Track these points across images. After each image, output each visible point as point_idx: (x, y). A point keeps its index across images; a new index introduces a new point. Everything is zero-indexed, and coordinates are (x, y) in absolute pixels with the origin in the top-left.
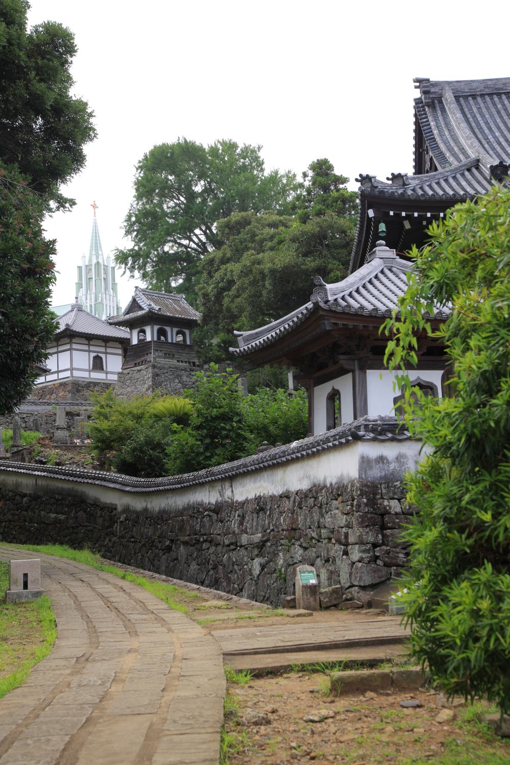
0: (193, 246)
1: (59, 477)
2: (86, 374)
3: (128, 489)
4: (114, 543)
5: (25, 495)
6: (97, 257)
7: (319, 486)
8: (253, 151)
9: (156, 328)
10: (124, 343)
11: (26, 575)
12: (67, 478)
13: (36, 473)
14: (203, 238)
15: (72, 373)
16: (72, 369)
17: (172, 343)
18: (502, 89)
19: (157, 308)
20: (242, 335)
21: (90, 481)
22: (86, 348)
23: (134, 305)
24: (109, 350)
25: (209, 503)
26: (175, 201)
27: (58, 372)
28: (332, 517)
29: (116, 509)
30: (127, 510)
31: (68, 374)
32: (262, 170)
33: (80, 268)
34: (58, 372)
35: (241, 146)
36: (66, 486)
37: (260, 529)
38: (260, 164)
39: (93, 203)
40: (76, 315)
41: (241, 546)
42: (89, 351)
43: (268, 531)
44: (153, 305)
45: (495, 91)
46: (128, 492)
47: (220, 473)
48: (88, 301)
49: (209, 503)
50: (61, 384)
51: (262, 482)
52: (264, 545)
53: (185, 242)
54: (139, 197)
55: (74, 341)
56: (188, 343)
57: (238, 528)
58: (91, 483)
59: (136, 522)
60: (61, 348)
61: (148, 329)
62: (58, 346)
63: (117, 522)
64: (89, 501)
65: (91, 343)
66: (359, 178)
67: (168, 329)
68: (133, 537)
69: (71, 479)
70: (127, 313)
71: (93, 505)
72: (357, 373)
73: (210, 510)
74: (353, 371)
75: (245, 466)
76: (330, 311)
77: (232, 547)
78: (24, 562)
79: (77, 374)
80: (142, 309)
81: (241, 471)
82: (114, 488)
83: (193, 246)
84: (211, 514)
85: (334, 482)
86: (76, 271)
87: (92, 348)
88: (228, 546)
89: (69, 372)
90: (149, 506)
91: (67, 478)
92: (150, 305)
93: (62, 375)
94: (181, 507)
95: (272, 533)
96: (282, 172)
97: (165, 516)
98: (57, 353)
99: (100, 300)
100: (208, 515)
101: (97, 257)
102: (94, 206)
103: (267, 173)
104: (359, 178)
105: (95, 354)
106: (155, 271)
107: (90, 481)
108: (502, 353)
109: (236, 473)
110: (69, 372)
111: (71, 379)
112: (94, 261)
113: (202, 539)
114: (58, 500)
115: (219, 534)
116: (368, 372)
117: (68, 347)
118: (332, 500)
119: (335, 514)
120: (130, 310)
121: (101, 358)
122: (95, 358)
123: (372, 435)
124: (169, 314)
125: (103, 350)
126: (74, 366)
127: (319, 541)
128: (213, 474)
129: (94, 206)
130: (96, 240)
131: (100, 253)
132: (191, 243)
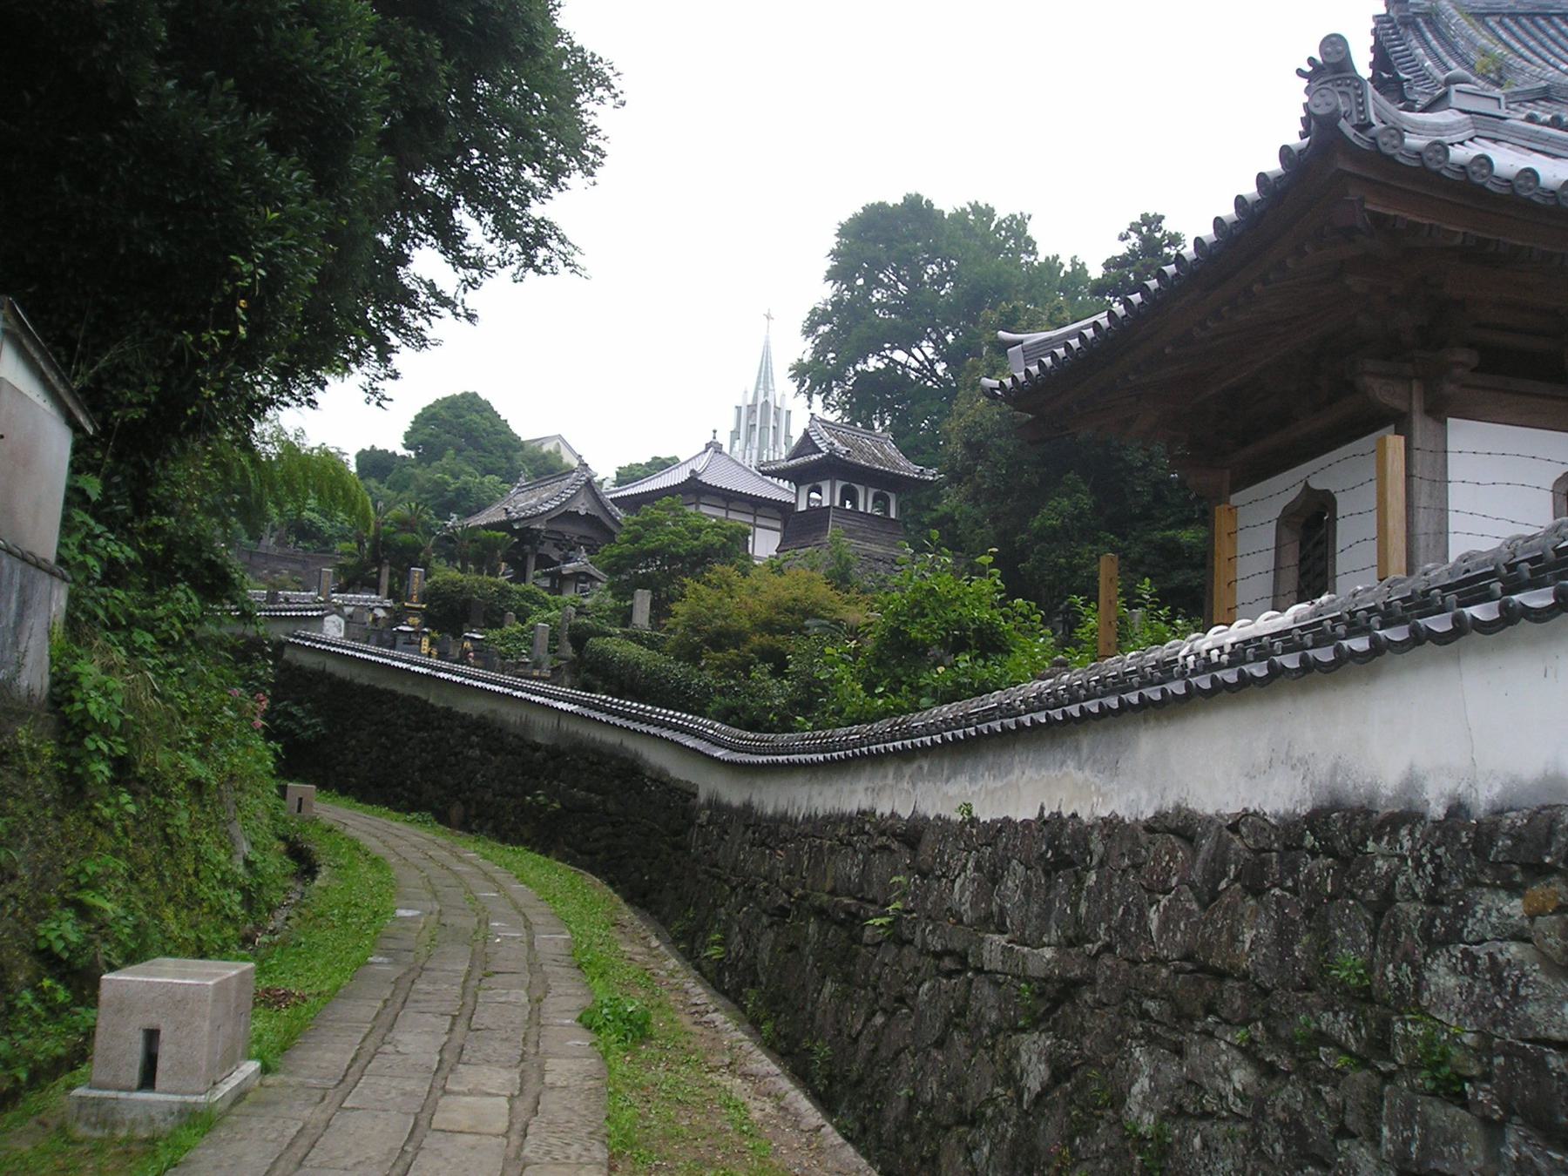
1: (598, 715)
3: (719, 753)
5: (536, 747)
6: (766, 394)
7: (1366, 812)
9: (839, 485)
10: (781, 510)
11: (152, 1036)
12: (612, 720)
13: (561, 705)
18: (1551, 8)
19: (844, 449)
20: (1021, 342)
21: (653, 730)
23: (807, 443)
24: (760, 521)
25: (893, 814)
29: (695, 795)
30: (716, 806)
32: (1034, 252)
33: (739, 408)
36: (611, 738)
41: (979, 970)
45: (1537, 10)
47: (928, 730)
51: (1071, 765)
53: (900, 356)
58: (654, 735)
61: (826, 487)
64: (648, 773)
66: (1308, 69)
69: (618, 722)
70: (789, 459)
71: (654, 781)
75: (1008, 711)
77: (948, 963)
78: (152, 976)
81: (996, 725)
82: (694, 750)
86: (734, 413)
88: (938, 956)
90: (755, 801)
91: (612, 720)
94: (821, 813)
95: (1107, 960)
97: (784, 828)
101: (766, 394)
102: (768, 317)
103: (1041, 259)
104: (1308, 69)
107: (653, 730)
109: (979, 732)
112: (761, 400)
114: (592, 763)
116: (1451, 422)
120: (796, 453)
125: (750, 519)
128: (909, 734)
129: (768, 317)
130: (766, 372)
132: (911, 359)
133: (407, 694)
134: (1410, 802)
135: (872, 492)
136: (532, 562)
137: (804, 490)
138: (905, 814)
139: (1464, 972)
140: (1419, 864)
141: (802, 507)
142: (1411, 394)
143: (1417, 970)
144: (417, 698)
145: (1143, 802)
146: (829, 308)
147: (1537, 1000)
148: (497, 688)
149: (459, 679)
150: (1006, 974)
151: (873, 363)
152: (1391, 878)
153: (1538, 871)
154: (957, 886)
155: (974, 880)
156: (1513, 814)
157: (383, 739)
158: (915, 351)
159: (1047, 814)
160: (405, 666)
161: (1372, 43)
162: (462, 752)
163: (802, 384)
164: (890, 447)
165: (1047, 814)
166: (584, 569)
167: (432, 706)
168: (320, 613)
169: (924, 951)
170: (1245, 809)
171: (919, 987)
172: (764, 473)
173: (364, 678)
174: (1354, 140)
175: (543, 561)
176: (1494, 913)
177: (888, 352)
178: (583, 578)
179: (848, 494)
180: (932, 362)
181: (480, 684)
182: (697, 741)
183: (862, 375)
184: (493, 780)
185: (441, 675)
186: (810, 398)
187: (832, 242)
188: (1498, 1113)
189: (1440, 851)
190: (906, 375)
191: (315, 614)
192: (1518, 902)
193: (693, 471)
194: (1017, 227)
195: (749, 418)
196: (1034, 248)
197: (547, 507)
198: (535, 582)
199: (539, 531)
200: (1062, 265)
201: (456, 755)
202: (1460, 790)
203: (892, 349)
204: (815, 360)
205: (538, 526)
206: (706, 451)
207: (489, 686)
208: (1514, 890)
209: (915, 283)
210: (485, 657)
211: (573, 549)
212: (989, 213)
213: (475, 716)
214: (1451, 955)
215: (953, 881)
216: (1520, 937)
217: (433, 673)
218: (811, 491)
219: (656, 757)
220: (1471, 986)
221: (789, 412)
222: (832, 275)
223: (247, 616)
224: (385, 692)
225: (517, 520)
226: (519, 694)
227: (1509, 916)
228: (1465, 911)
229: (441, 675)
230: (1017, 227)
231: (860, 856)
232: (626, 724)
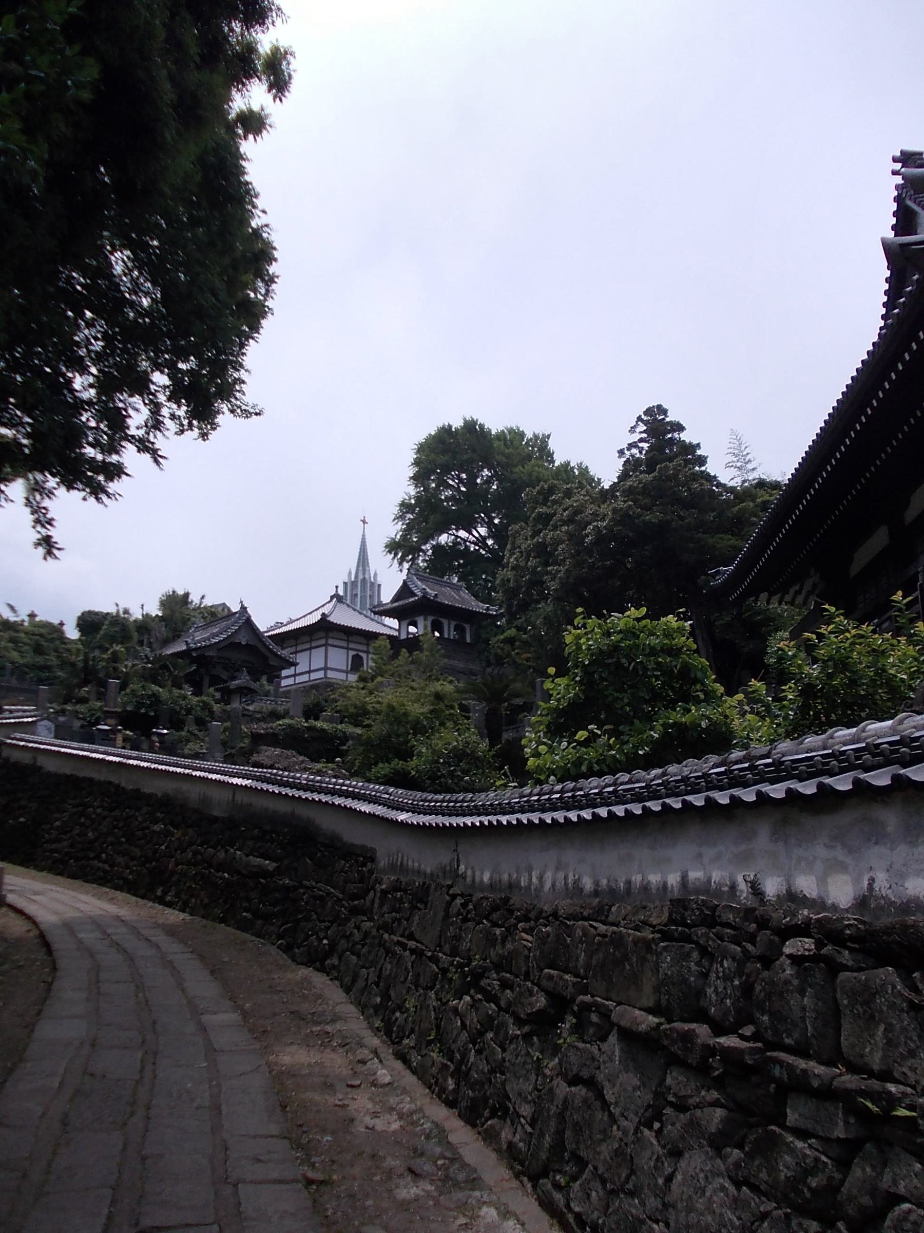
2: (342, 676)
4: (366, 934)
5: (216, 819)
6: (364, 573)
9: (430, 618)
13: (235, 781)
16: (326, 669)
17: (448, 639)
19: (433, 593)
22: (344, 644)
29: (373, 860)
31: (320, 674)
32: (553, 462)
34: (309, 672)
35: (529, 435)
36: (283, 808)
40: (335, 607)
42: (348, 649)
46: (403, 824)
50: (312, 687)
54: (417, 479)
55: (331, 635)
56: (468, 640)
59: (421, 901)
61: (421, 621)
62: (311, 641)
63: (373, 888)
65: (350, 639)
67: (445, 622)
68: (411, 937)
80: (417, 596)
87: (351, 645)
89: (323, 672)
91: (284, 791)
93: (314, 676)
98: (310, 649)
101: (364, 573)
102: (364, 522)
105: (355, 653)
110: (323, 672)
111: (324, 680)
112: (361, 577)
117: (323, 642)
120: (398, 597)
121: (361, 658)
122: (353, 656)
124: (447, 602)
125: (365, 648)
126: (329, 666)
129: (364, 522)
131: (367, 569)
132: (471, 536)
133: (102, 779)
135: (453, 624)
136: (206, 680)
137: (404, 623)
141: (403, 636)
144: (110, 783)
146: (413, 501)
148: (179, 770)
149: (145, 764)
151: (444, 539)
157: (82, 820)
160: (101, 756)
161: (895, 209)
162: (148, 828)
163: (396, 555)
164: (464, 592)
166: (246, 685)
167: (123, 789)
168: (34, 719)
173: (67, 769)
175: (215, 681)
177: (454, 531)
178: (245, 691)
179: (436, 626)
181: (164, 767)
182: (371, 805)
183: (437, 548)
184: (176, 850)
185: (131, 762)
186: (400, 564)
187: (412, 456)
190: (467, 548)
191: (30, 720)
193: (323, 614)
194: (541, 443)
195: (352, 590)
196: (552, 458)
197: (216, 640)
198: (211, 694)
199: (212, 657)
201: (143, 829)
203: (457, 530)
204: (404, 537)
205: (211, 654)
206: (331, 601)
207: (171, 769)
209: (471, 483)
210: (169, 748)
211: (238, 671)
212: (522, 435)
213: (159, 795)
217: (125, 761)
218: (410, 624)
219: (327, 823)
221: (379, 586)
223: (546, 912)
224: (85, 779)
225: (196, 649)
226: (198, 773)
229: (131, 762)
230: (541, 443)
232: (297, 793)
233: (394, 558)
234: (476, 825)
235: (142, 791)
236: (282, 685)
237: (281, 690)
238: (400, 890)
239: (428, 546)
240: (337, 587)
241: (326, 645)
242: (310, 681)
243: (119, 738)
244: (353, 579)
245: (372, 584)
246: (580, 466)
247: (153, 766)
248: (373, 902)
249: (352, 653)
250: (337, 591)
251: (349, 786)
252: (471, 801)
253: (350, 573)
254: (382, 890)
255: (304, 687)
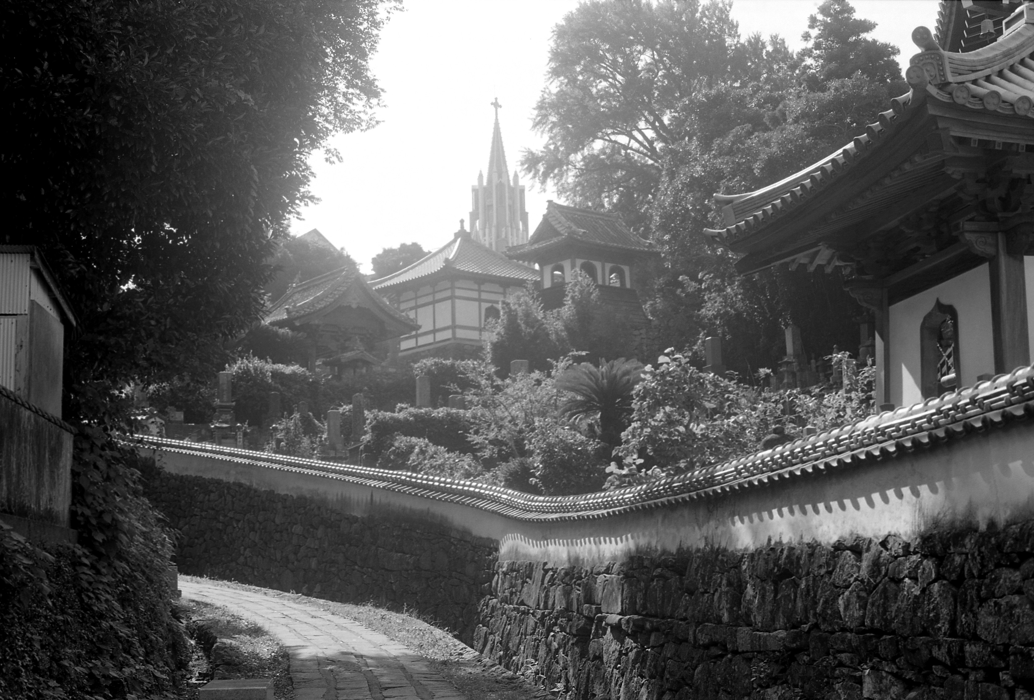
0: (635, 145)
4: (494, 608)
5: (356, 520)
6: (500, 176)
8: (722, 11)
9: (579, 262)
13: (373, 483)
14: (650, 134)
15: (454, 333)
16: (454, 327)
22: (475, 295)
26: (610, 80)
27: (434, 331)
28: (998, 613)
31: (447, 334)
32: (736, 35)
34: (434, 331)
37: (781, 621)
38: (733, 27)
39: (494, 101)
41: (735, 652)
42: (480, 300)
43: (806, 627)
44: (574, 228)
46: (516, 519)
48: (487, 238)
49: (664, 552)
52: (792, 659)
53: (623, 139)
55: (457, 284)
56: (628, 286)
57: (730, 611)
60: (439, 296)
63: (497, 573)
65: (483, 288)
67: (598, 265)
68: (522, 603)
72: (1003, 260)
73: (664, 564)
74: (993, 262)
76: (953, 106)
77: (715, 651)
79: (461, 334)
80: (562, 235)
82: (494, 512)
83: (635, 145)
84: (668, 574)
85: (1002, 518)
87: (484, 296)
88: (706, 647)
92: (570, 228)
93: (440, 336)
95: (814, 633)
96: (766, 38)
98: (434, 303)
99: (503, 236)
100: (660, 576)
101: (500, 176)
102: (496, 105)
105: (489, 305)
106: (579, 184)
108: (185, 643)
111: (452, 341)
112: (495, 181)
113: (648, 626)
115: (684, 619)
116: (1026, 258)
117: (448, 293)
118: (998, 565)
119: (1012, 607)
122: (488, 310)
123: (117, 563)
126: (458, 322)
127: (953, 670)
129: (496, 105)
132: (632, 141)
134: (970, 523)
138: (673, 549)
139: (996, 614)
140: (974, 558)
142: (997, 241)
143: (975, 615)
145: (832, 533)
147: (1027, 624)
150: (753, 652)
152: (962, 566)
153: (1024, 556)
154: (716, 597)
155: (727, 593)
156: (1014, 527)
158: (635, 133)
159: (773, 542)
165: (773, 542)
169: (696, 646)
170: (890, 532)
171: (694, 670)
172: (511, 258)
174: (937, 96)
176: (1008, 581)
180: (651, 142)
186: (543, 182)
188: (1011, 683)
189: (983, 549)
192: (1018, 573)
193: (447, 260)
200: (764, 46)
202: (993, 514)
208: (1016, 567)
214: (989, 606)
215: (713, 594)
216: (1019, 592)
220: (999, 622)
222: (555, 73)
227: (1015, 581)
228: (996, 579)
231: (642, 584)
233: (534, 177)
234: (735, 489)
235: (276, 493)
236: (402, 348)
237: (400, 354)
238: (515, 571)
239: (579, 156)
240: (462, 222)
241: (452, 298)
242: (435, 343)
243: (240, 436)
244: (485, 183)
245: (512, 190)
246: (774, 40)
247: (286, 468)
248: (497, 583)
249: (485, 305)
250: (462, 227)
251: (476, 487)
252: (560, 502)
253: (481, 176)
254: (503, 572)
255: (429, 350)
